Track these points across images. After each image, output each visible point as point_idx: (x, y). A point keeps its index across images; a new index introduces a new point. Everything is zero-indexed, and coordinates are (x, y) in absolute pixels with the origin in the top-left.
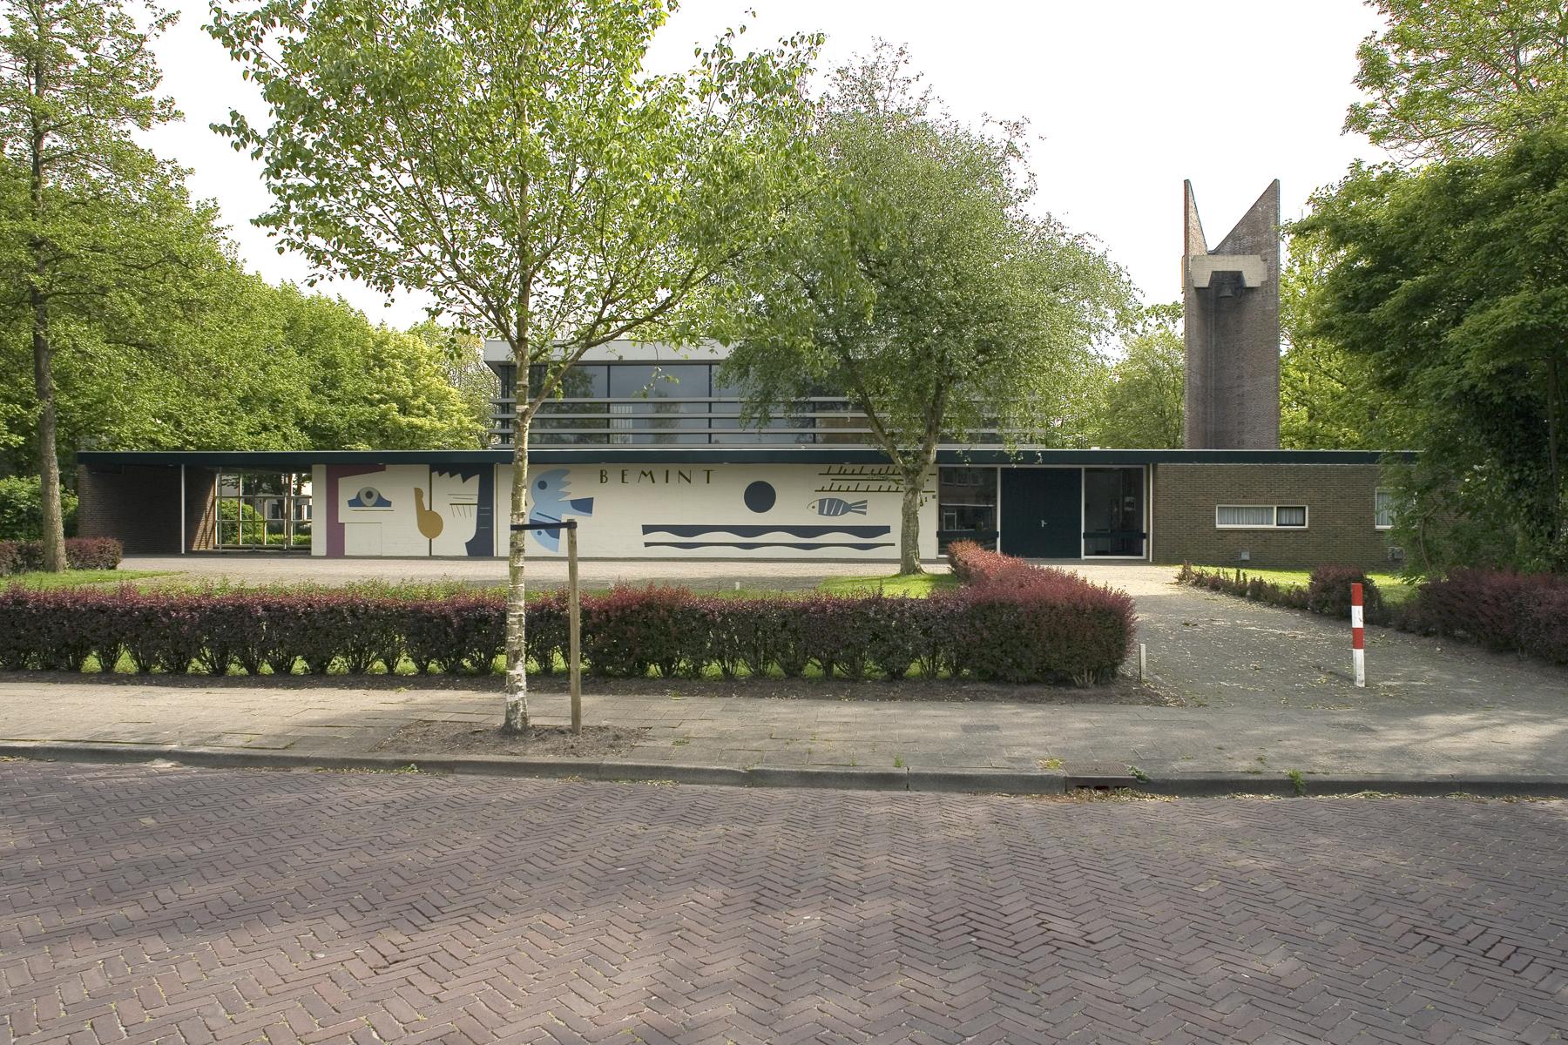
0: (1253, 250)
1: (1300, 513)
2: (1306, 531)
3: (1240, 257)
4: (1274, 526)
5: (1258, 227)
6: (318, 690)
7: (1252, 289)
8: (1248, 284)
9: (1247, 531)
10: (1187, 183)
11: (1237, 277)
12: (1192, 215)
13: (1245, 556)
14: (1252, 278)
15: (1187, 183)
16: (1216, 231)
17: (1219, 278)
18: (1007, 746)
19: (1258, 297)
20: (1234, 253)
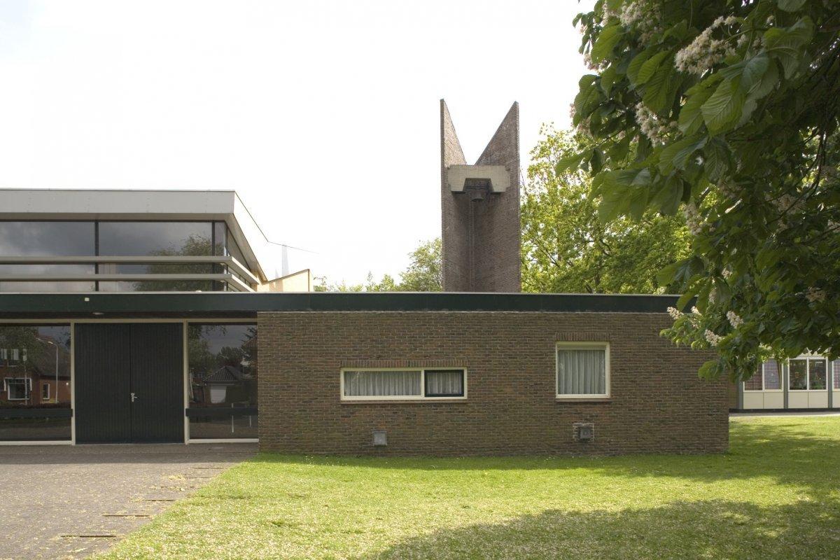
0: (499, 162)
1: (457, 381)
2: (464, 404)
3: (490, 167)
4: (422, 397)
5: (504, 145)
6: (70, 465)
7: (499, 194)
8: (496, 189)
9: (384, 405)
10: (442, 102)
11: (487, 183)
12: (447, 130)
13: (380, 440)
14: (499, 185)
15: (442, 102)
16: (472, 149)
17: (471, 184)
18: (750, 438)
19: (504, 201)
20: (487, 164)
